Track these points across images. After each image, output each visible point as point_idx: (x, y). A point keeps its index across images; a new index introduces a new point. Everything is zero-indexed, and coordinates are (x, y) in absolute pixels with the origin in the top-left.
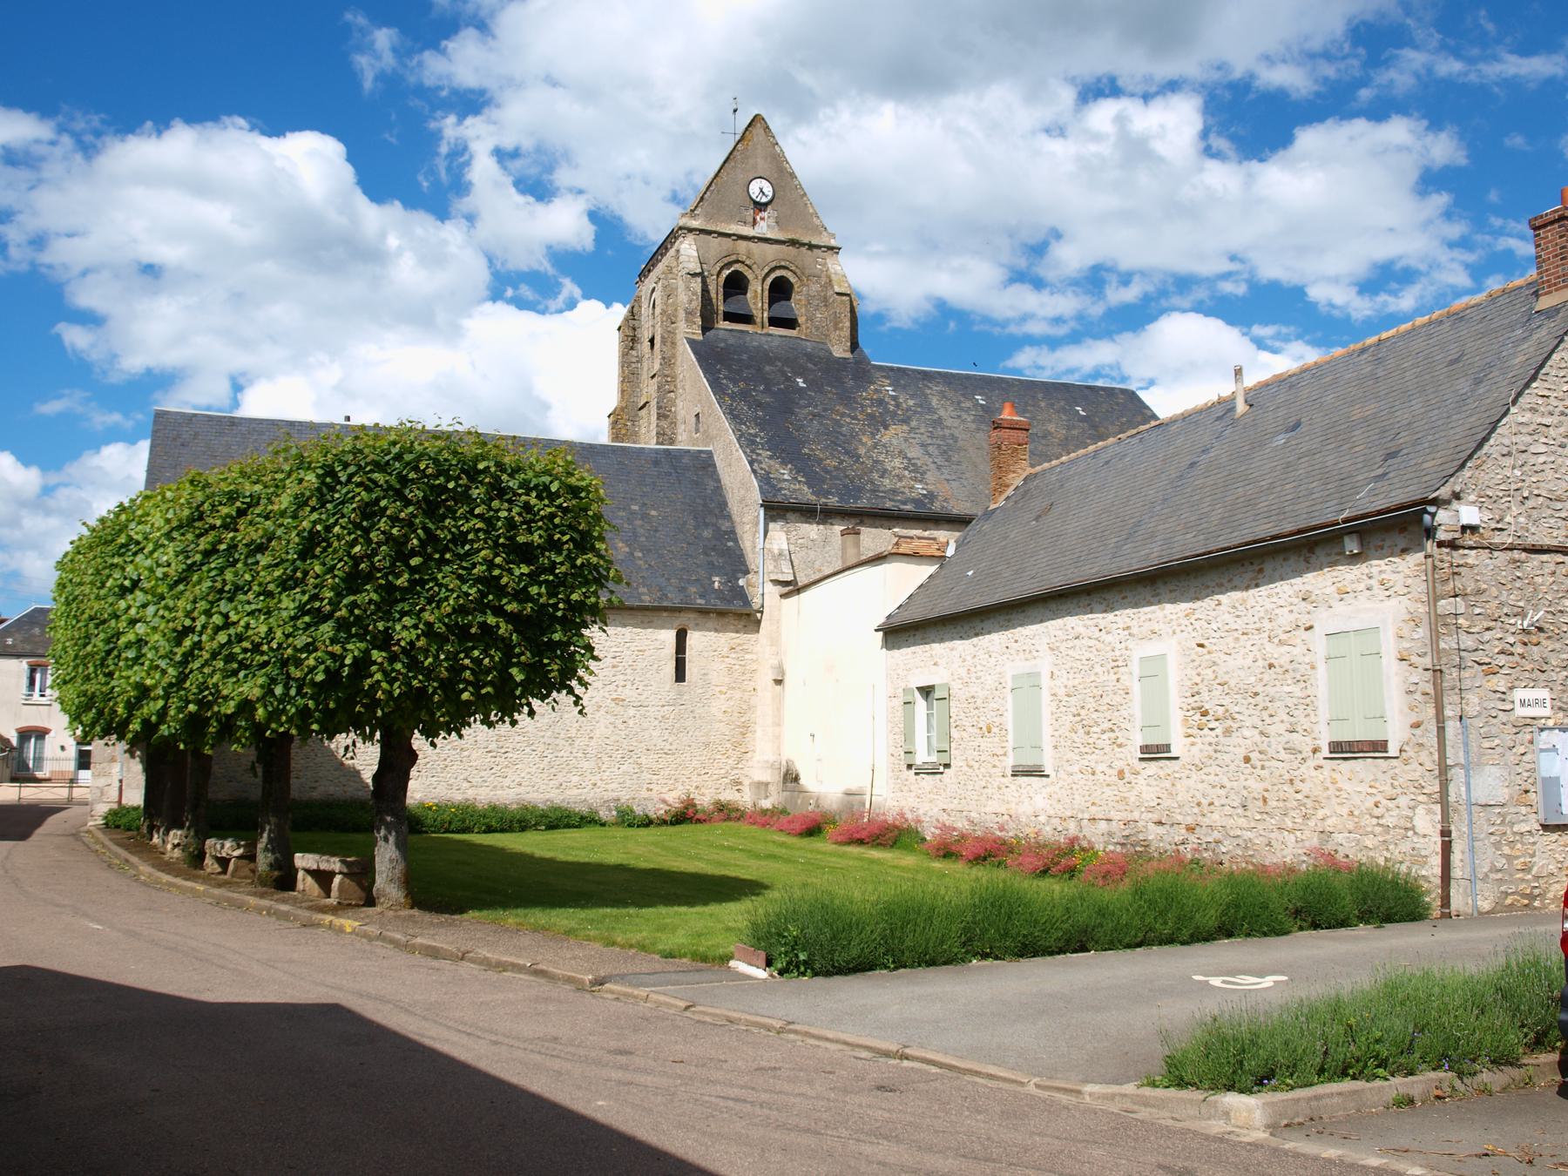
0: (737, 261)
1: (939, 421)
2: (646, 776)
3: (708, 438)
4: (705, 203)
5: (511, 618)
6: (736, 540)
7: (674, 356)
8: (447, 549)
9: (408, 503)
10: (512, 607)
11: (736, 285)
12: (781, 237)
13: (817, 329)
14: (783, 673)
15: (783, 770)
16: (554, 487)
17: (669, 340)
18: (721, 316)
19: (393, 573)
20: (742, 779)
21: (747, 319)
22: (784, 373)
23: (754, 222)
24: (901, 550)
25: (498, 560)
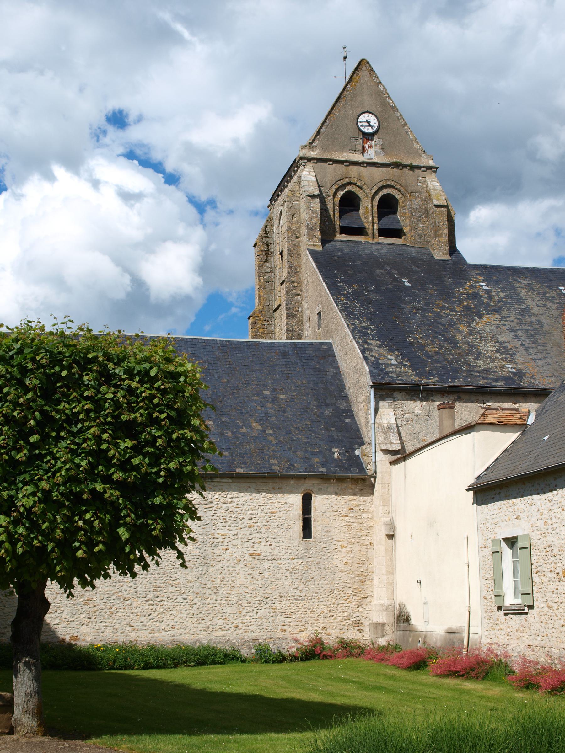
0: (350, 183)
1: (527, 310)
2: (280, 619)
3: (329, 333)
4: (321, 136)
5: (117, 485)
6: (352, 417)
7: (299, 265)
8: (62, 428)
9: (27, 390)
10: (118, 476)
11: (350, 203)
12: (386, 161)
13: (420, 236)
14: (394, 529)
15: (397, 612)
16: (153, 373)
17: (294, 252)
18: (338, 230)
19: (14, 448)
20: (363, 620)
21: (360, 231)
22: (392, 275)
23: (363, 150)
24: (487, 420)
25: (105, 436)
